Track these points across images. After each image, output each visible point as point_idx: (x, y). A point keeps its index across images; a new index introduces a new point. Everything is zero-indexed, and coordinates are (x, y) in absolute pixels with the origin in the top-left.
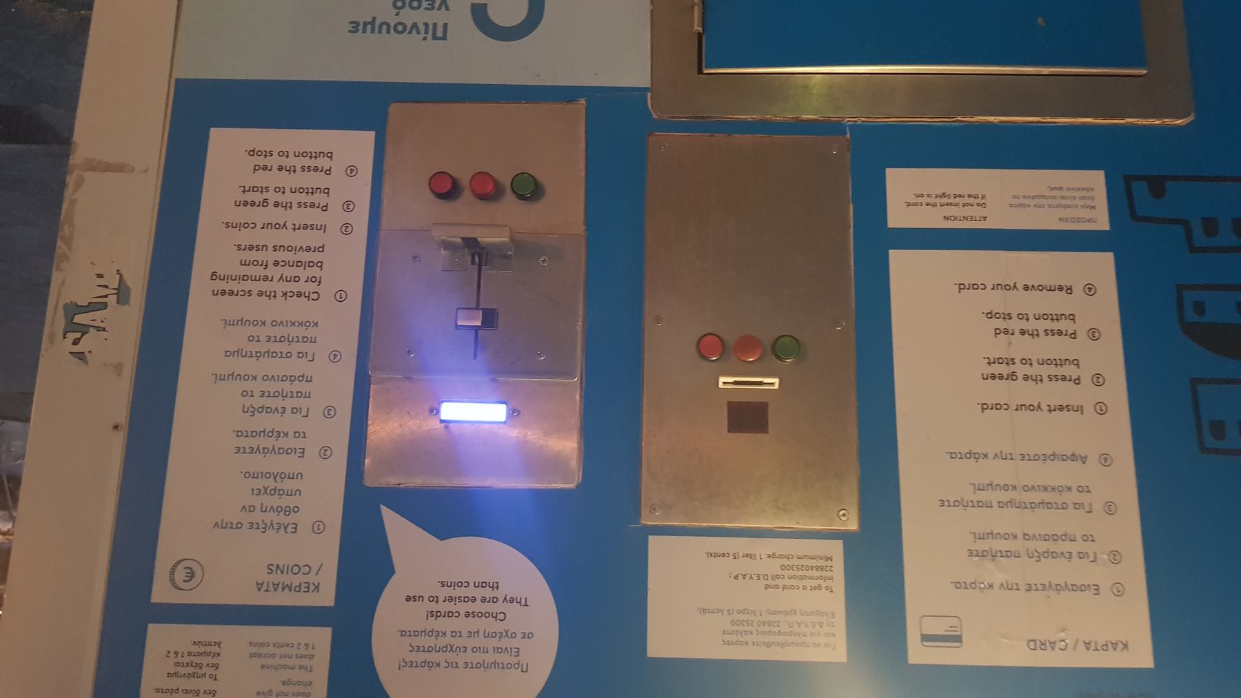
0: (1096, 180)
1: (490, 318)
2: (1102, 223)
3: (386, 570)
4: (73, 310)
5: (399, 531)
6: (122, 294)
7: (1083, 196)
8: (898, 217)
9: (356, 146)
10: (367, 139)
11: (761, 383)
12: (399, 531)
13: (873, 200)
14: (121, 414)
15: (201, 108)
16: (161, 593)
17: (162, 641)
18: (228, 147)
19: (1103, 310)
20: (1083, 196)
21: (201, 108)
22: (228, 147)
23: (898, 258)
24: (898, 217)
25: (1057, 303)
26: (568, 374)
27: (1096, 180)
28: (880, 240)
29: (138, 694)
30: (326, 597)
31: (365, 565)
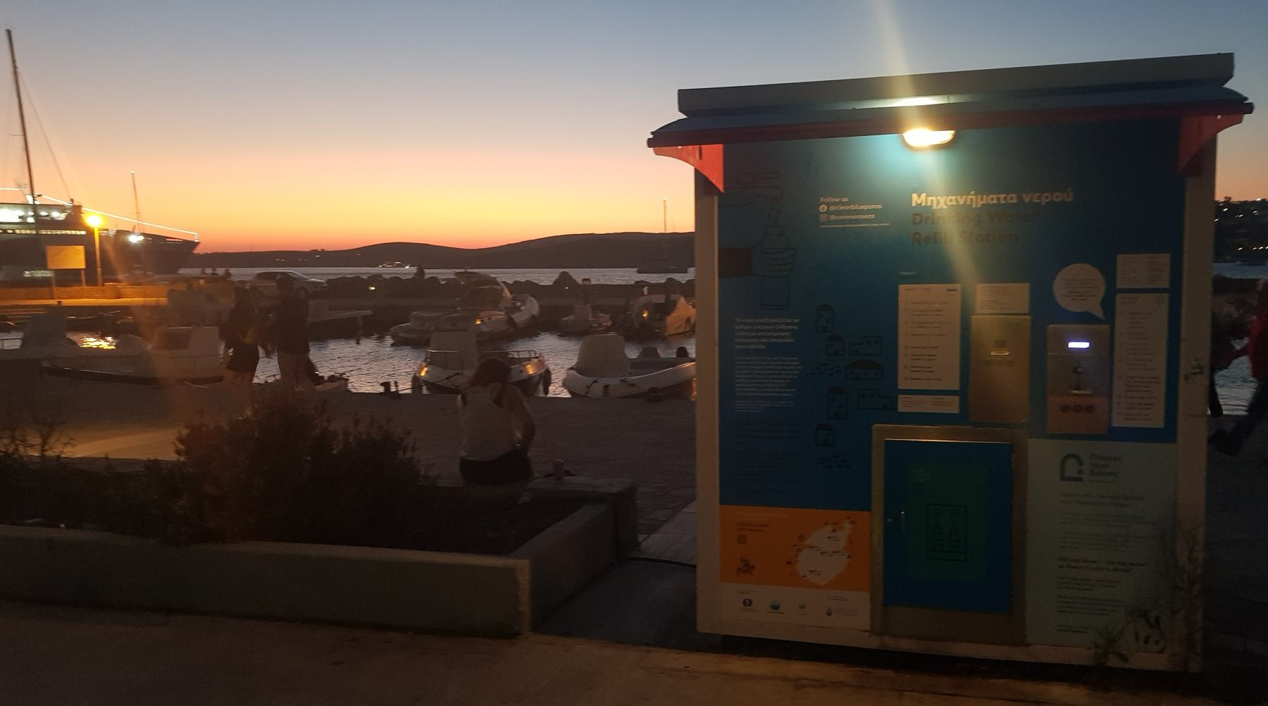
0: (901, 409)
1: (1075, 371)
2: (900, 396)
3: (1103, 303)
4: (1201, 373)
5: (1099, 313)
6: (1186, 378)
7: (905, 405)
8: (956, 399)
9: (1117, 422)
10: (1115, 424)
11: (18, 307)
12: (1099, 313)
13: (963, 404)
14: (1183, 344)
15: (1167, 434)
16: (1166, 296)
17: (1165, 284)
18: (1157, 420)
19: (902, 373)
20: (905, 405)
21: (1167, 434)
22: (1157, 420)
23: (957, 388)
24: (956, 399)
25: (917, 375)
26: (866, 506)
27: (901, 409)
28: (963, 393)
29: (1267, 205)
30: (1119, 296)
31: (1108, 304)
